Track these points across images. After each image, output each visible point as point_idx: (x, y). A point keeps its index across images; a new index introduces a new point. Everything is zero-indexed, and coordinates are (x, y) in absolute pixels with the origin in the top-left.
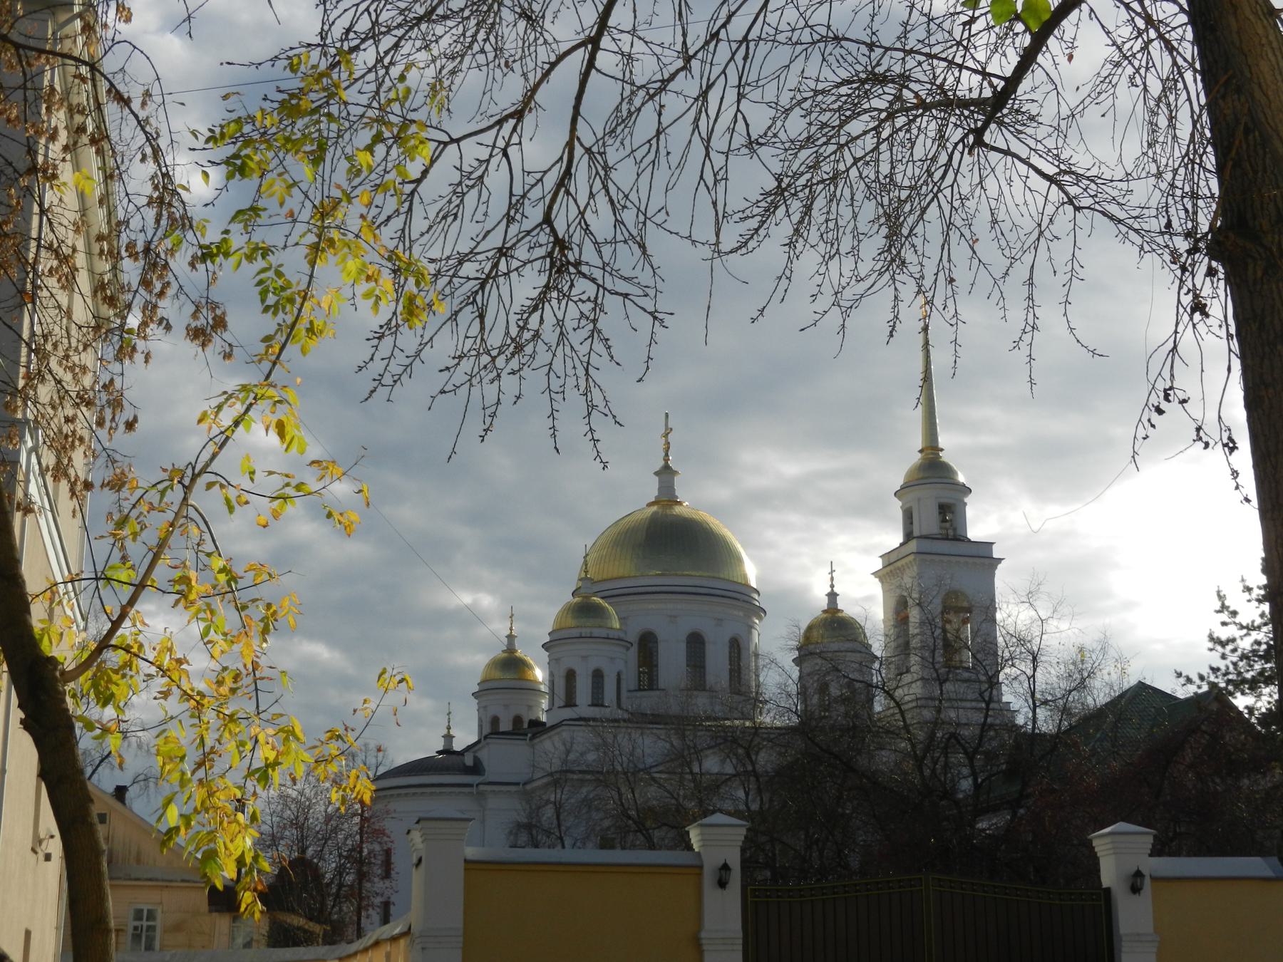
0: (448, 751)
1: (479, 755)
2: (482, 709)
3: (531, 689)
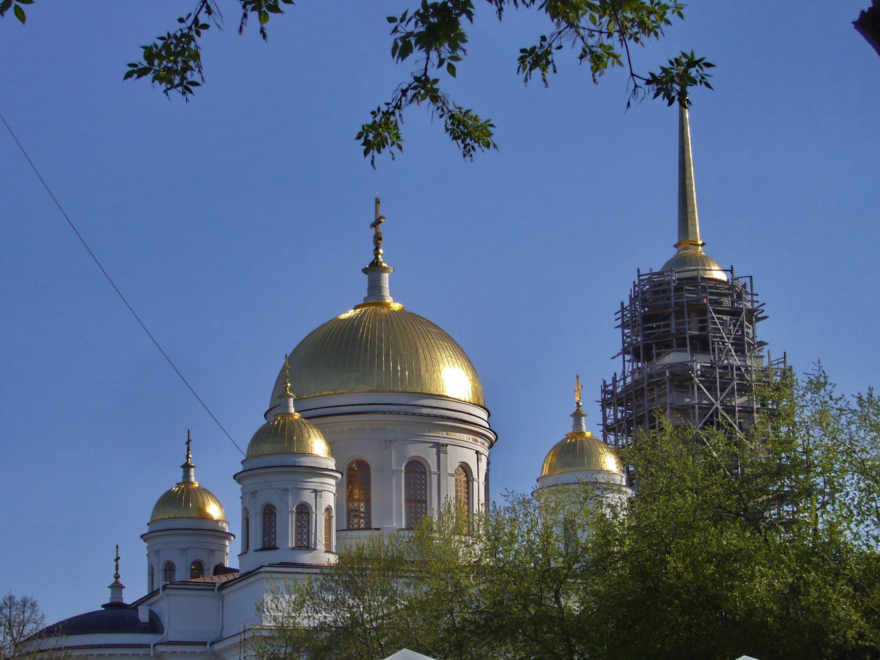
0: (115, 606)
1: (155, 609)
2: (153, 553)
3: (600, 486)
